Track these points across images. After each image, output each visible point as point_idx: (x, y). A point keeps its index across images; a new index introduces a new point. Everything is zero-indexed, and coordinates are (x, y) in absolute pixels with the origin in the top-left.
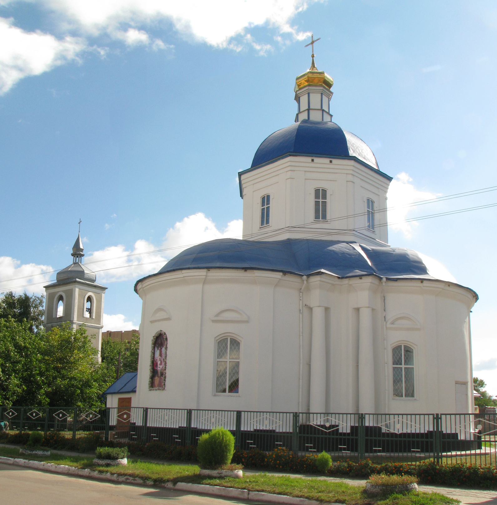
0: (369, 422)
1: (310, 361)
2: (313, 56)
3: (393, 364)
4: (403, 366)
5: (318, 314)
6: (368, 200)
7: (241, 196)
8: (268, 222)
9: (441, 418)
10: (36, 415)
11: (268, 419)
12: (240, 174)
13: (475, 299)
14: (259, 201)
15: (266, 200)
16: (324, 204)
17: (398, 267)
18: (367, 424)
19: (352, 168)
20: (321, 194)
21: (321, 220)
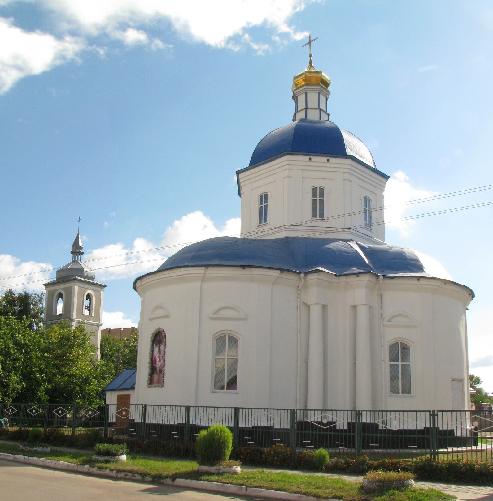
1: (308, 359)
2: (310, 56)
3: (390, 361)
4: (400, 363)
5: (316, 311)
6: (365, 199)
7: (239, 194)
8: (265, 220)
9: (437, 415)
11: (266, 416)
12: (238, 173)
13: (471, 297)
14: (257, 199)
15: (264, 198)
16: (322, 202)
18: (364, 421)
20: (318, 193)
21: (318, 218)
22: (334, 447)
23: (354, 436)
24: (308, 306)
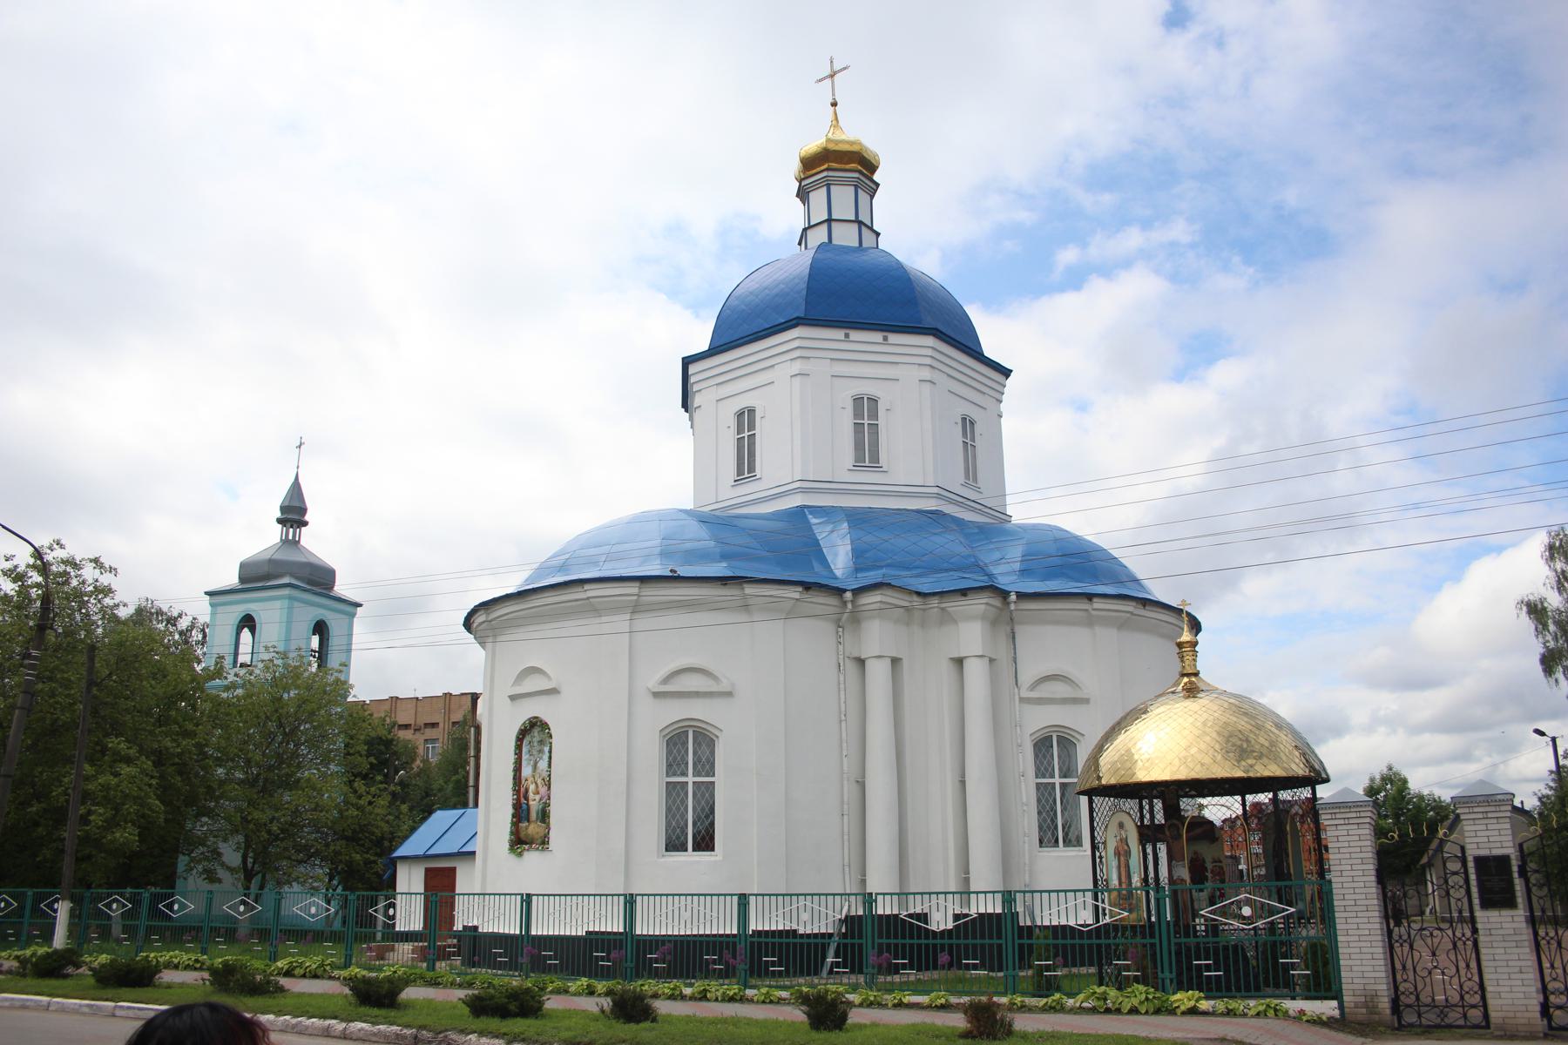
0: (884, 908)
5: (878, 673)
6: (964, 419)
7: (685, 405)
8: (752, 469)
10: (172, 904)
11: (942, 909)
12: (687, 362)
14: (732, 422)
15: (746, 418)
17: (1077, 578)
18: (880, 912)
19: (930, 352)
20: (866, 407)
22: (959, 968)
23: (860, 945)
24: (861, 662)
